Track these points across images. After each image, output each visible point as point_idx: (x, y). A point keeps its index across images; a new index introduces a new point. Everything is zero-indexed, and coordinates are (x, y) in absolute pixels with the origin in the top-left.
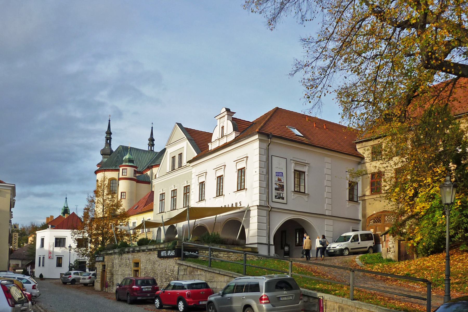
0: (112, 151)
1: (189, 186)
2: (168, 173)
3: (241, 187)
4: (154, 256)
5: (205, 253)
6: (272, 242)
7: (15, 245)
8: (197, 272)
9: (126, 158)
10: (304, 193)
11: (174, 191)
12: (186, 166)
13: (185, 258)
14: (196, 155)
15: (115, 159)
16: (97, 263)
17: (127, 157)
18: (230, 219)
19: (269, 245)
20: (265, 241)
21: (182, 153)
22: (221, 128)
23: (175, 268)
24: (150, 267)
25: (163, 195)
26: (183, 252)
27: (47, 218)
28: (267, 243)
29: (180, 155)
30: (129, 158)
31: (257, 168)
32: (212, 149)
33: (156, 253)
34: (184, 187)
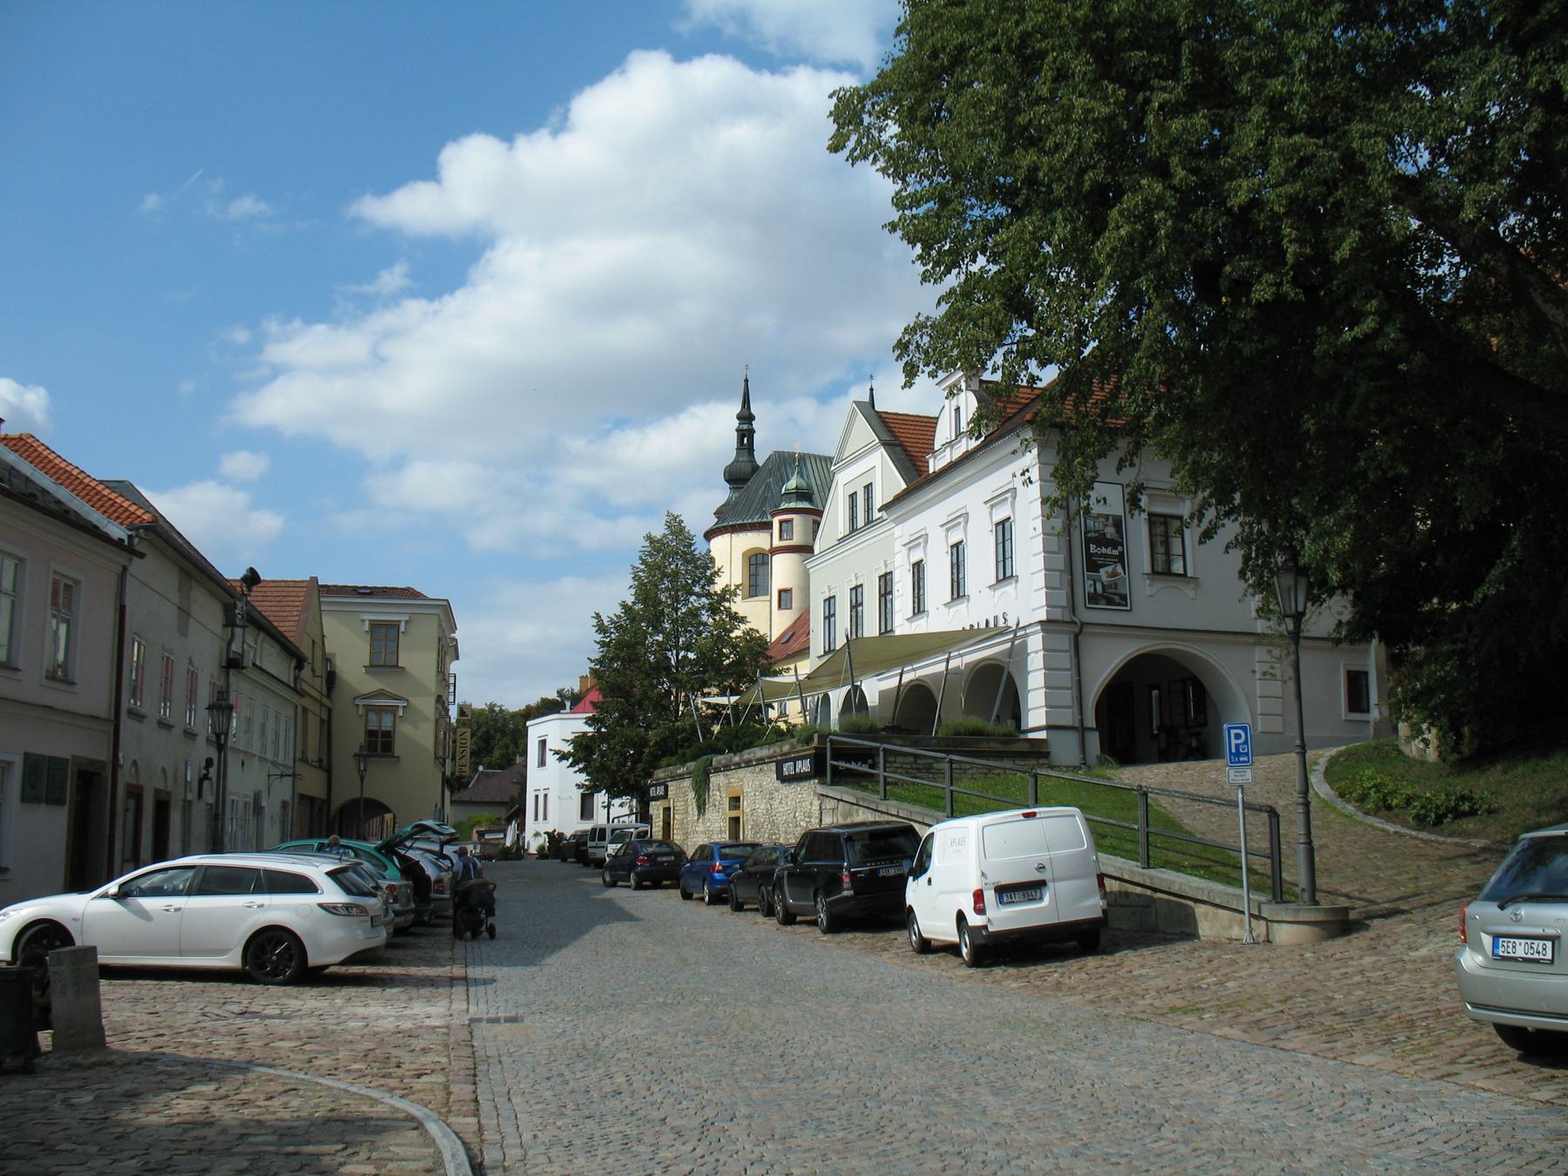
0: (755, 468)
1: (891, 573)
2: (841, 540)
3: (1005, 575)
4: (768, 777)
5: (895, 762)
6: (1091, 721)
7: (463, 762)
8: (858, 815)
9: (789, 487)
10: (1185, 575)
11: (857, 589)
12: (881, 520)
13: (839, 777)
14: (904, 486)
15: (761, 492)
16: (653, 803)
17: (792, 483)
18: (983, 663)
19: (1082, 730)
20: (1068, 718)
21: (871, 484)
22: (953, 412)
23: (814, 808)
24: (763, 806)
25: (830, 601)
26: (829, 762)
27: (582, 677)
28: (1077, 724)
29: (868, 488)
30: (797, 488)
31: (1037, 518)
32: (937, 469)
33: (773, 766)
34: (880, 577)
